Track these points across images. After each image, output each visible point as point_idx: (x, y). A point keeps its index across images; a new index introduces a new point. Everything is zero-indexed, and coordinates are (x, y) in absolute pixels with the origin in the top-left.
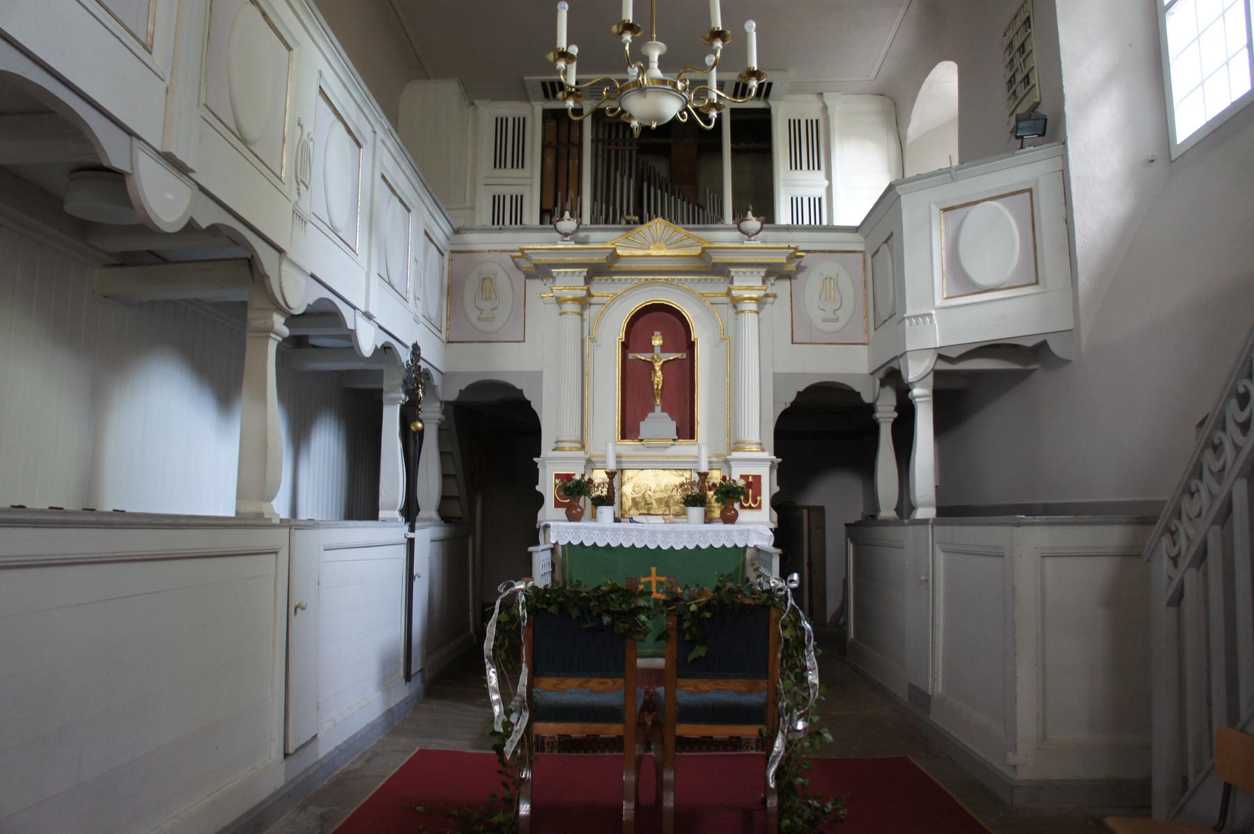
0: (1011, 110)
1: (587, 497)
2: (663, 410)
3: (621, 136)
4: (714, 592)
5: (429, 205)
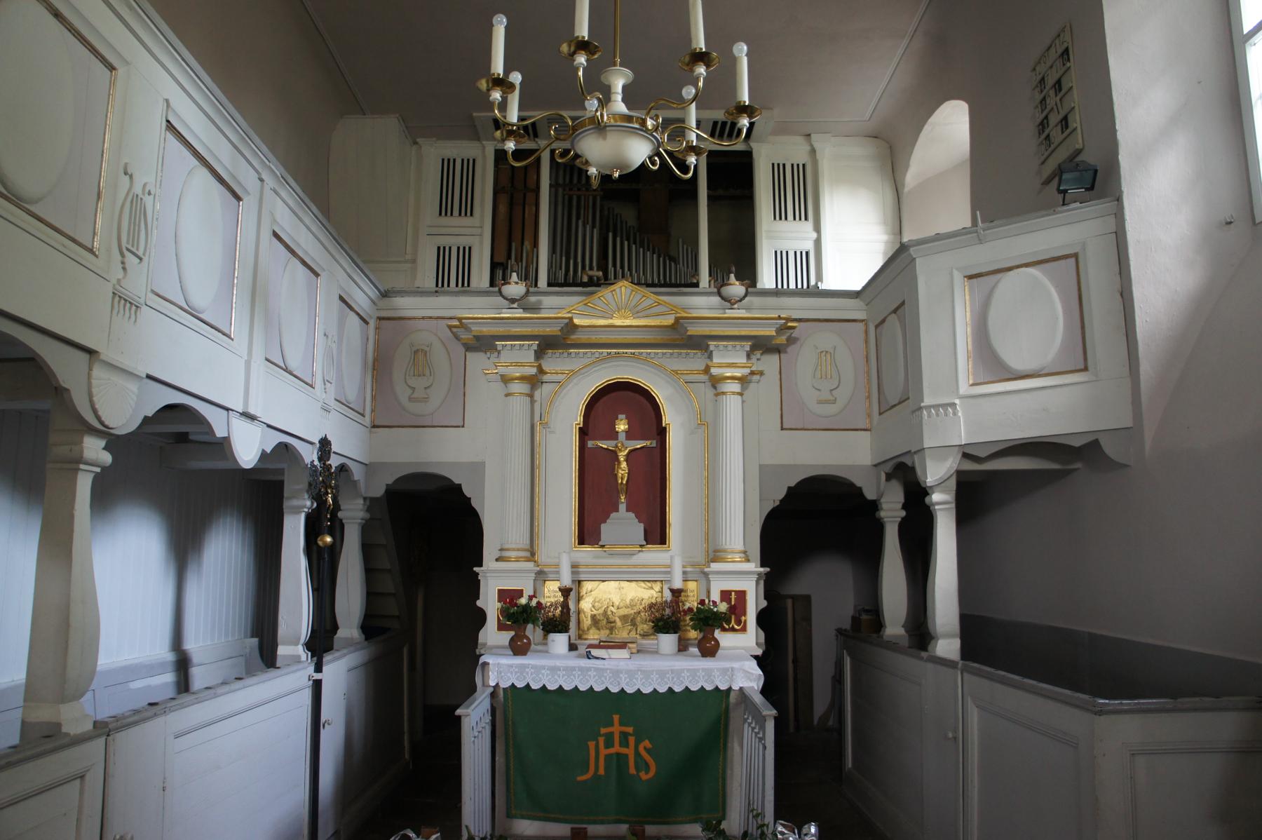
0: (1043, 158)
2: (628, 510)
3: (575, 181)
5: (346, 266)
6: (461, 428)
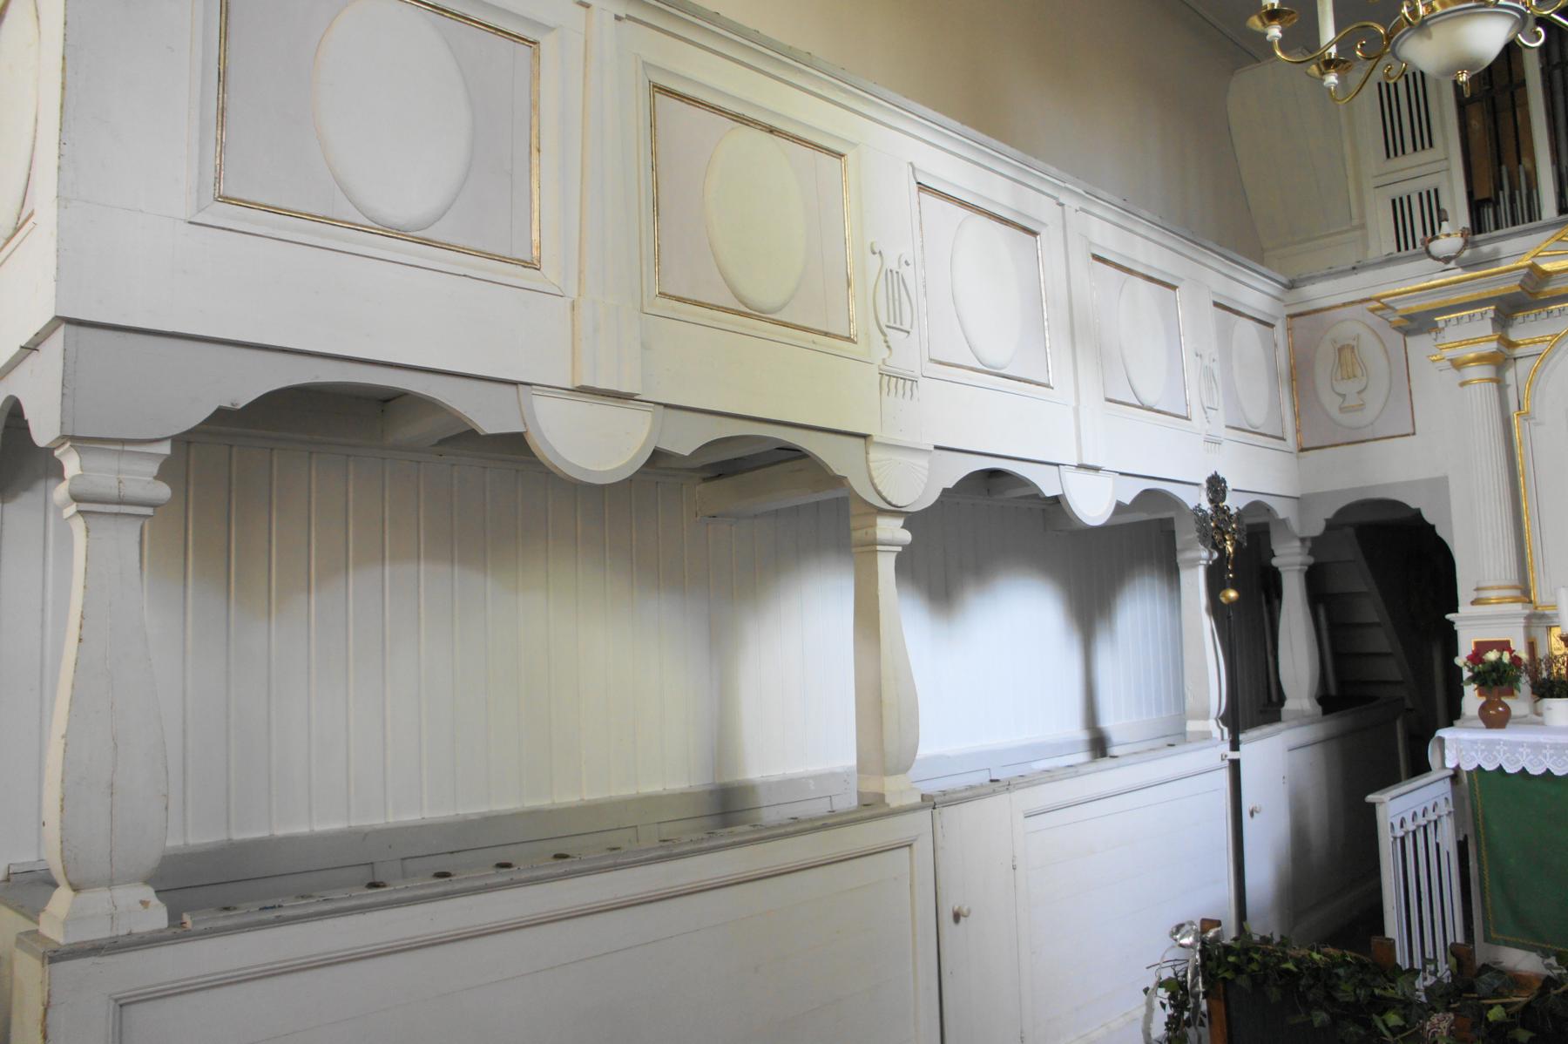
5: (1216, 265)
6: (1412, 437)
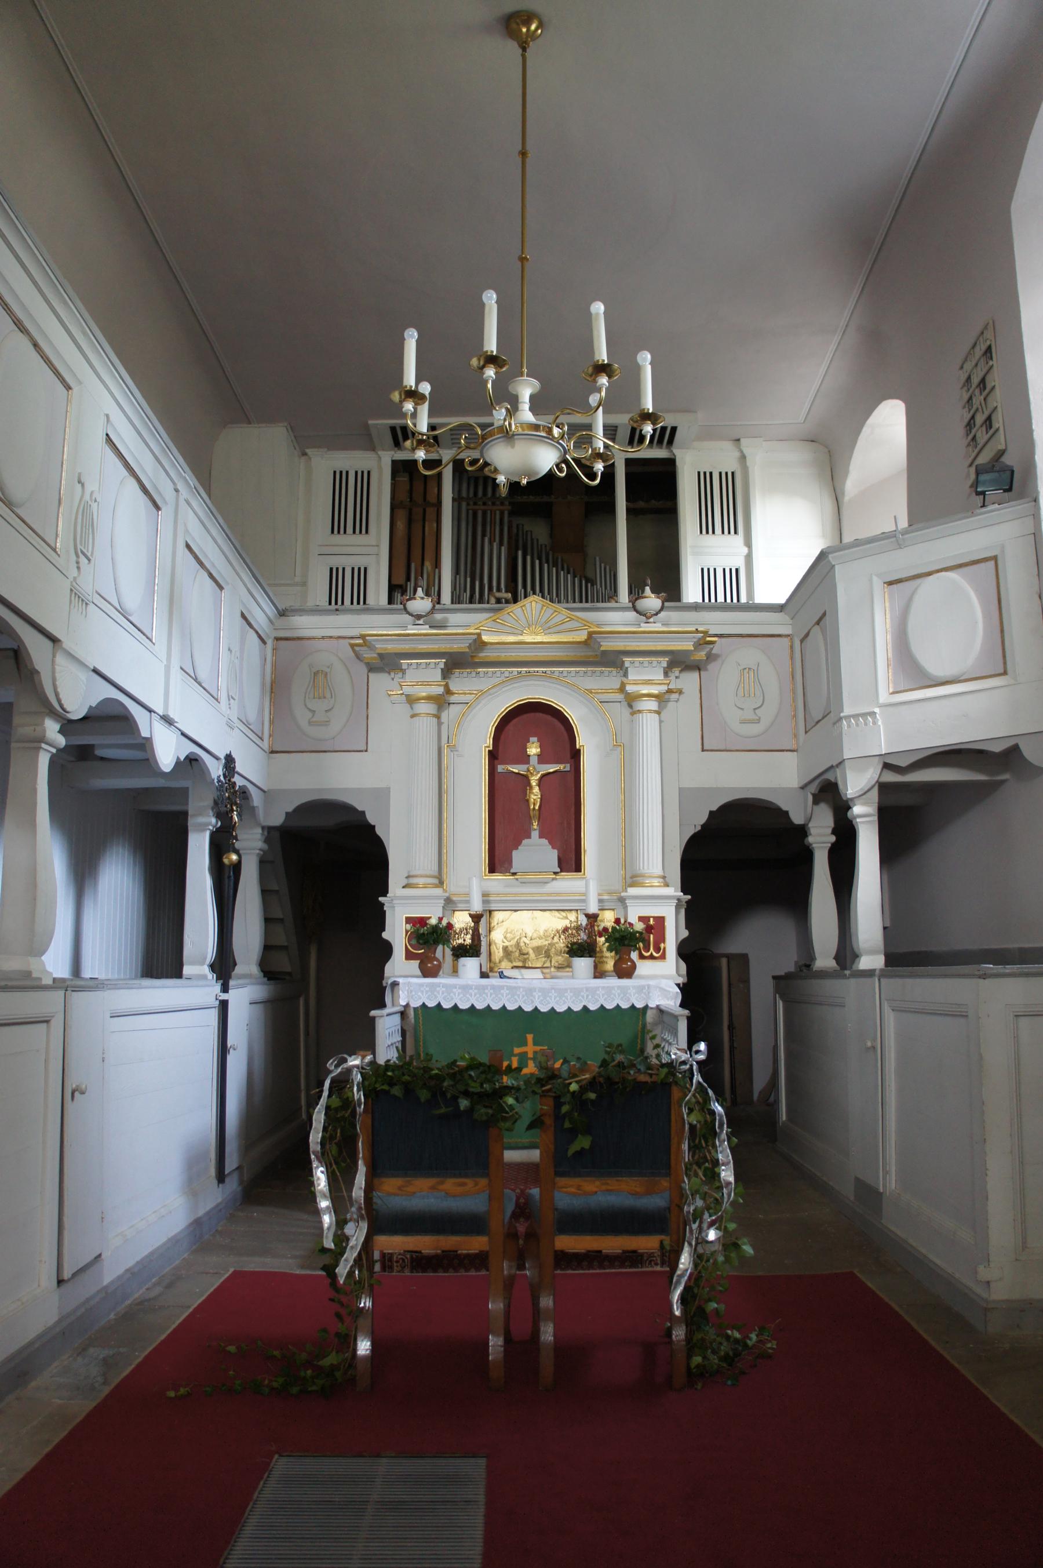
1: (445, 946)
2: (541, 837)
3: (480, 493)
4: (600, 1067)
